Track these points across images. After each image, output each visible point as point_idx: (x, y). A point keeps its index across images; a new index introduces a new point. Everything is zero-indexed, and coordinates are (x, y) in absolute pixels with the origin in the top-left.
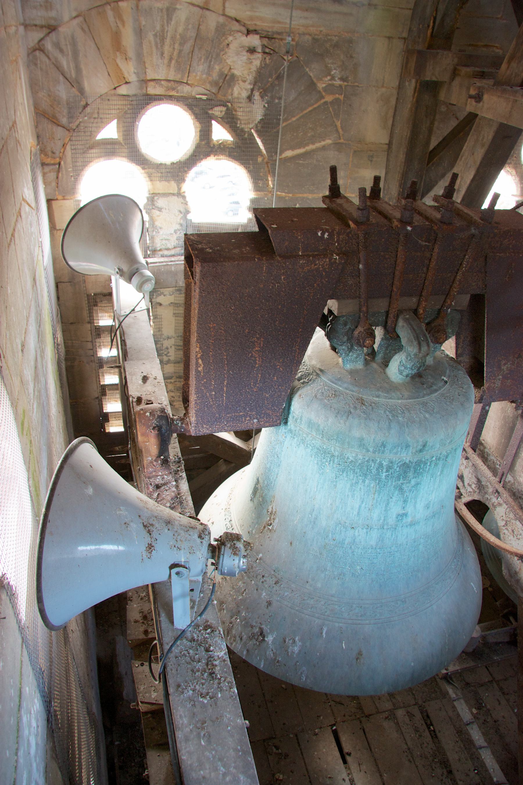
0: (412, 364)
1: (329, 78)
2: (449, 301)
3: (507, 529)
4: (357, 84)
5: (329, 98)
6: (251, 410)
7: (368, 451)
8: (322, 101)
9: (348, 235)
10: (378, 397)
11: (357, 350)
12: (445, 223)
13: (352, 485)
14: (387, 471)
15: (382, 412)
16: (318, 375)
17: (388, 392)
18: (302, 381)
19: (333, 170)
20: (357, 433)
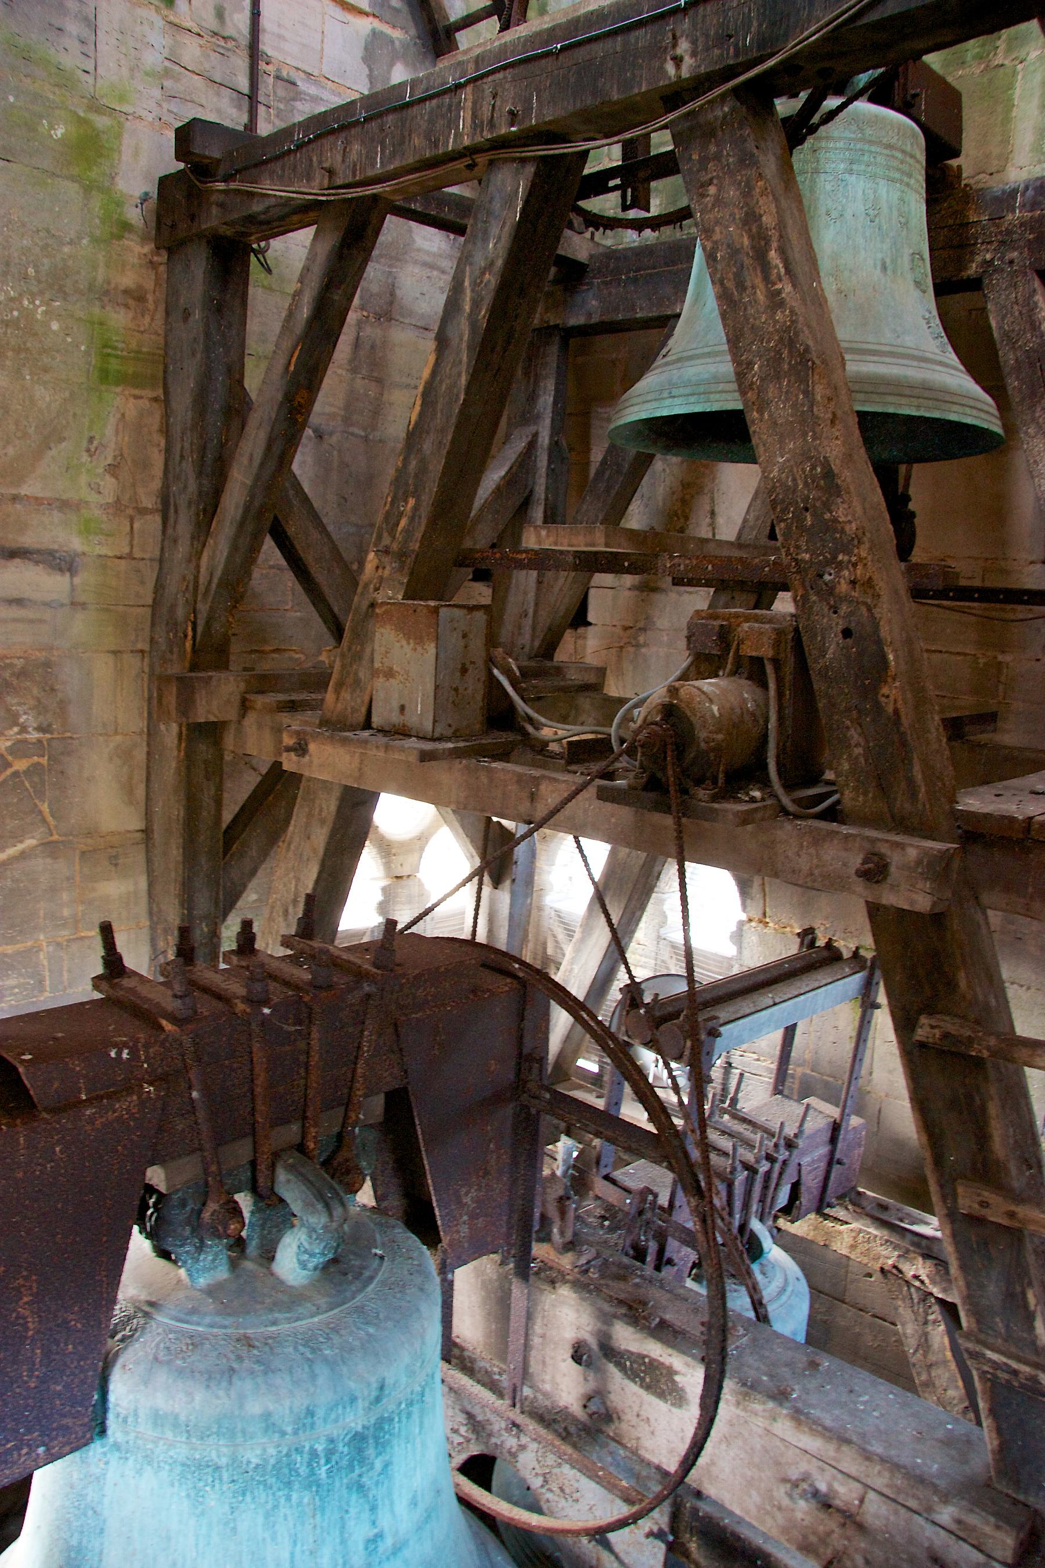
0: (323, 1245)
1: (16, 729)
2: (353, 1115)
3: (550, 1490)
4: (69, 734)
5: (21, 765)
6: (29, 1431)
7: (283, 1433)
8: (9, 771)
9: (162, 1044)
10: (274, 1323)
11: (211, 1246)
12: (321, 987)
13: (267, 1515)
14: (328, 1461)
15: (291, 1349)
16: (147, 1315)
17: (289, 1309)
18: (119, 1336)
19: (107, 931)
20: (254, 1407)
